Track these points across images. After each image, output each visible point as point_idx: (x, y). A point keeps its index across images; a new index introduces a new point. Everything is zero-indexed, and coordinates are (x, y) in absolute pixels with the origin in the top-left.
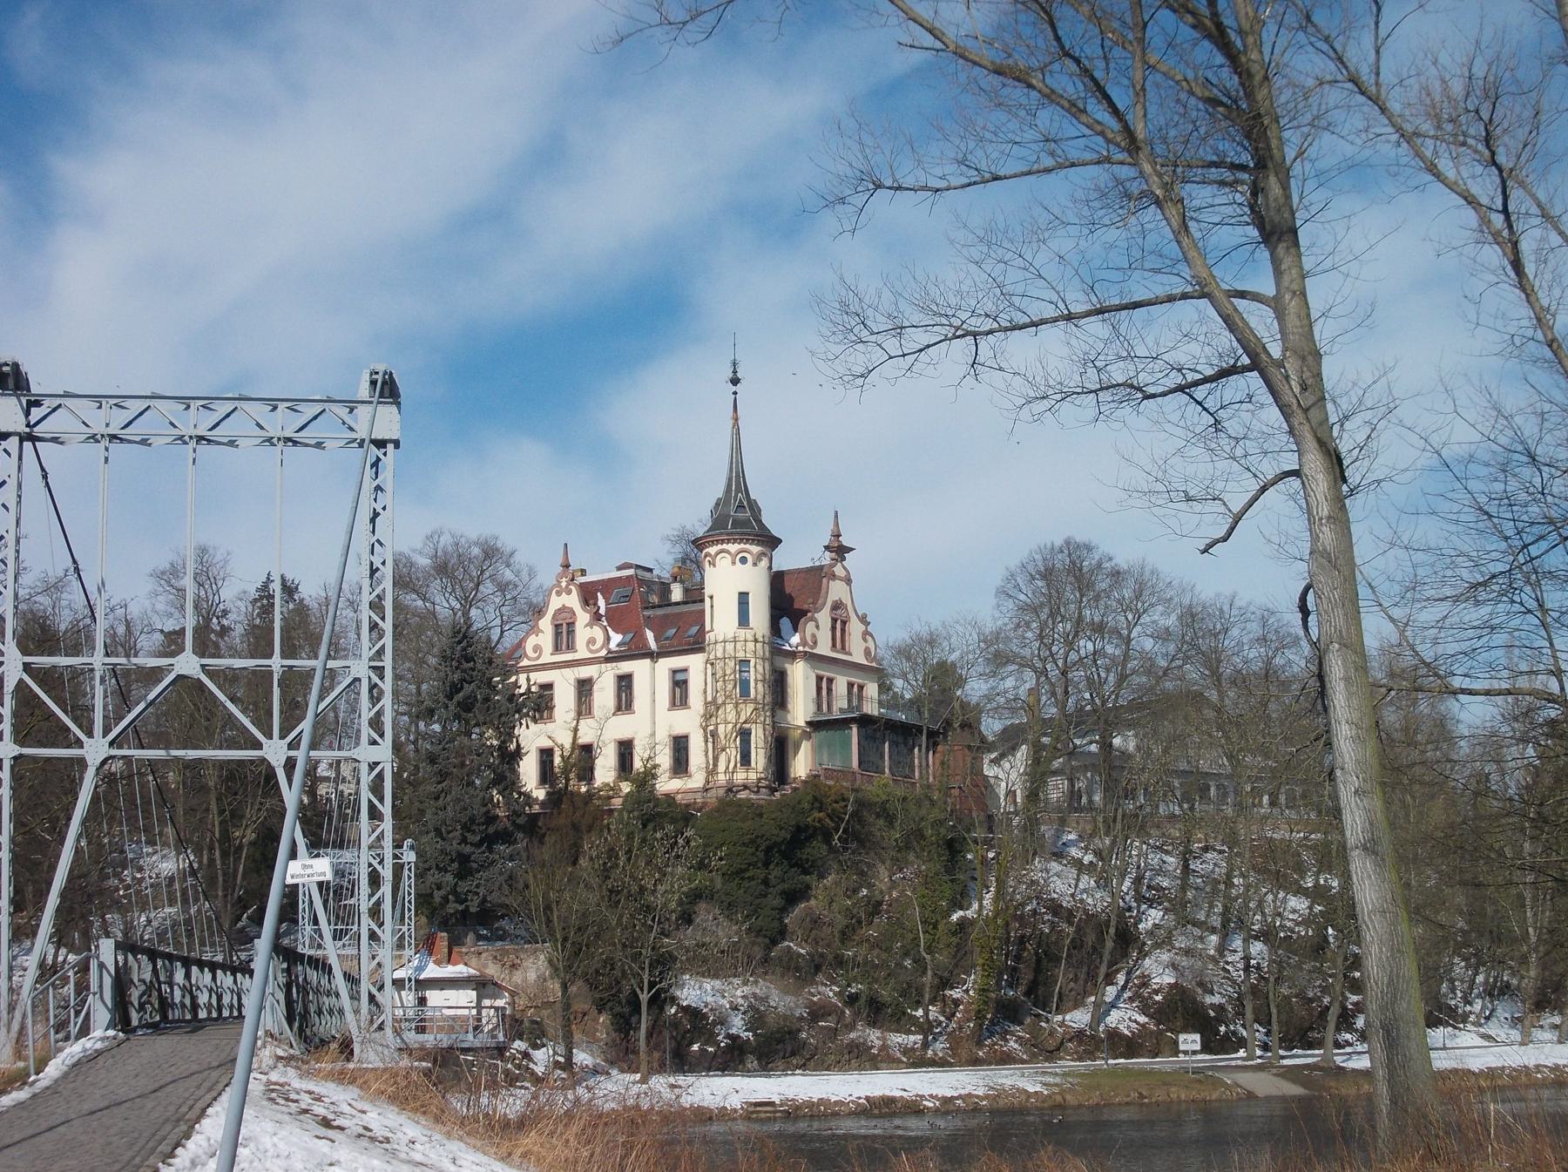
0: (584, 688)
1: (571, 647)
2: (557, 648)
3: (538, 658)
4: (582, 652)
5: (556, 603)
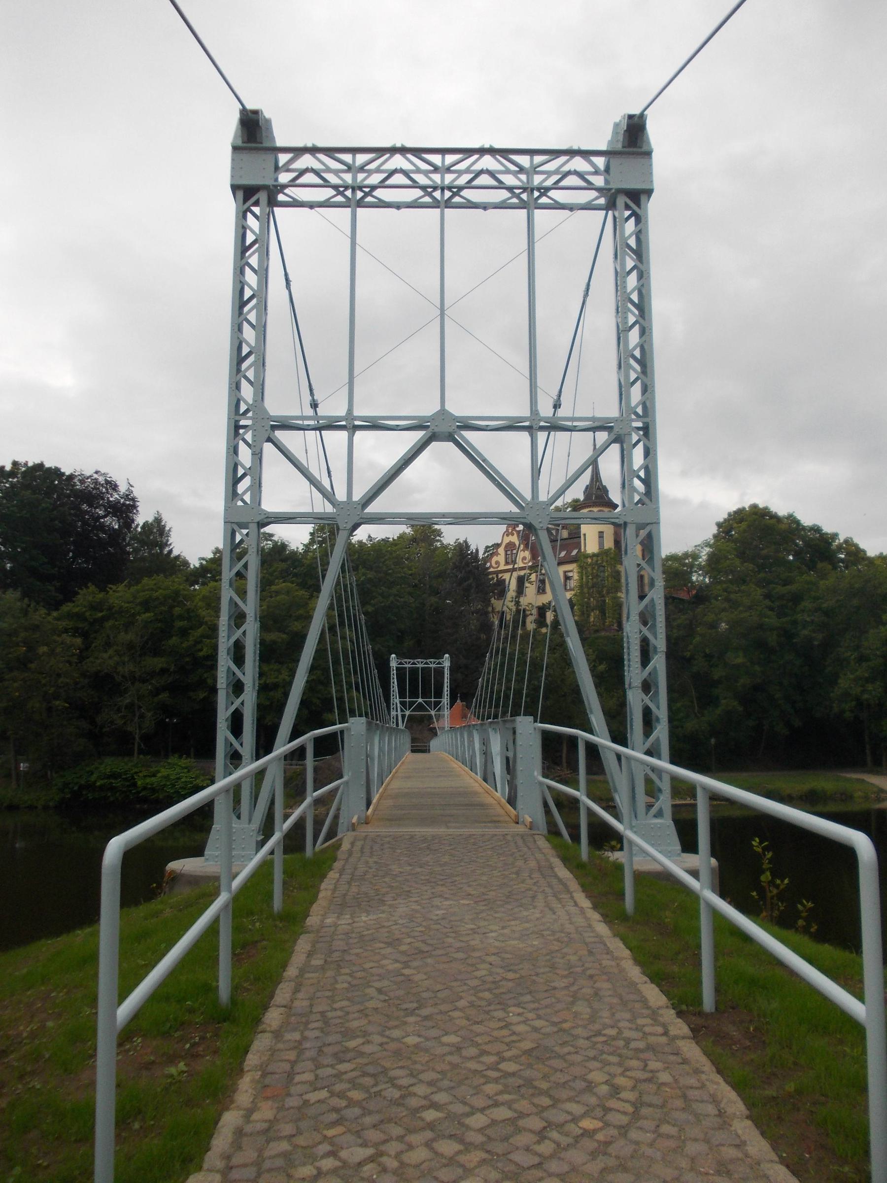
0: (521, 581)
1: (514, 562)
2: (507, 563)
3: (498, 567)
4: (520, 564)
5: (507, 540)
